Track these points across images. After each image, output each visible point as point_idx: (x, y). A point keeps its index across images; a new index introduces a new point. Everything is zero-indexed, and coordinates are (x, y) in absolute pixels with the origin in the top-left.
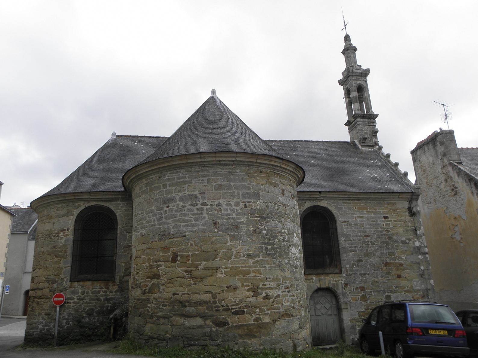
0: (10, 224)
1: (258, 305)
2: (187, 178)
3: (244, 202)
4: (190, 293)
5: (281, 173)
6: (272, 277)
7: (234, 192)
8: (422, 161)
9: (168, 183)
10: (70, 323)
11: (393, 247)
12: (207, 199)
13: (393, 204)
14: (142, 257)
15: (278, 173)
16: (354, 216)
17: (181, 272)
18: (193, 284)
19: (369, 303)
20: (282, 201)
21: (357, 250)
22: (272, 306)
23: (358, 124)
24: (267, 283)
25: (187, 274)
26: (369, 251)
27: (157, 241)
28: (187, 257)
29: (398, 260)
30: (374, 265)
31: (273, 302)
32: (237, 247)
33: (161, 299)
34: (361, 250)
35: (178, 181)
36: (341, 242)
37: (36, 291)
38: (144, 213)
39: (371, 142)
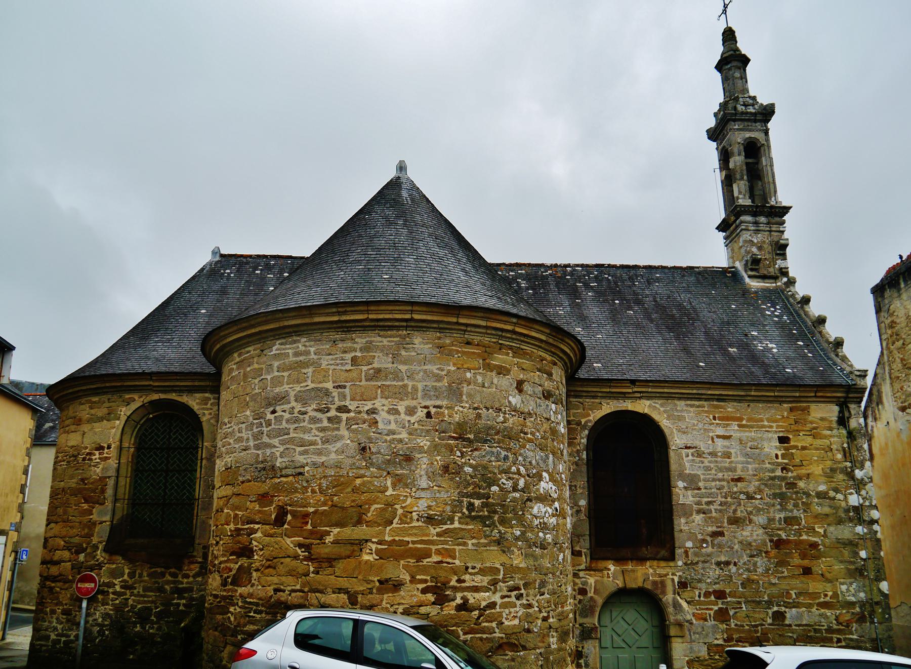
0: (31, 428)
1: (445, 622)
2: (312, 353)
3: (425, 407)
4: (306, 589)
5: (518, 346)
6: (478, 566)
7: (405, 386)
8: (894, 312)
9: (276, 364)
10: (107, 632)
11: (796, 506)
12: (348, 398)
13: (802, 410)
14: (226, 511)
15: (511, 346)
16: (711, 434)
17: (292, 546)
18: (313, 573)
19: (733, 626)
20: (516, 404)
21: (713, 511)
22: (476, 626)
23: (743, 227)
24: (467, 577)
25: (302, 552)
26: (739, 514)
27: (250, 481)
28: (303, 516)
29: (807, 534)
30: (750, 544)
31: (479, 618)
32: (406, 500)
33: (253, 599)
34: (720, 511)
35: (294, 359)
36: (677, 490)
37: (49, 566)
38: (233, 423)
39: (771, 270)
